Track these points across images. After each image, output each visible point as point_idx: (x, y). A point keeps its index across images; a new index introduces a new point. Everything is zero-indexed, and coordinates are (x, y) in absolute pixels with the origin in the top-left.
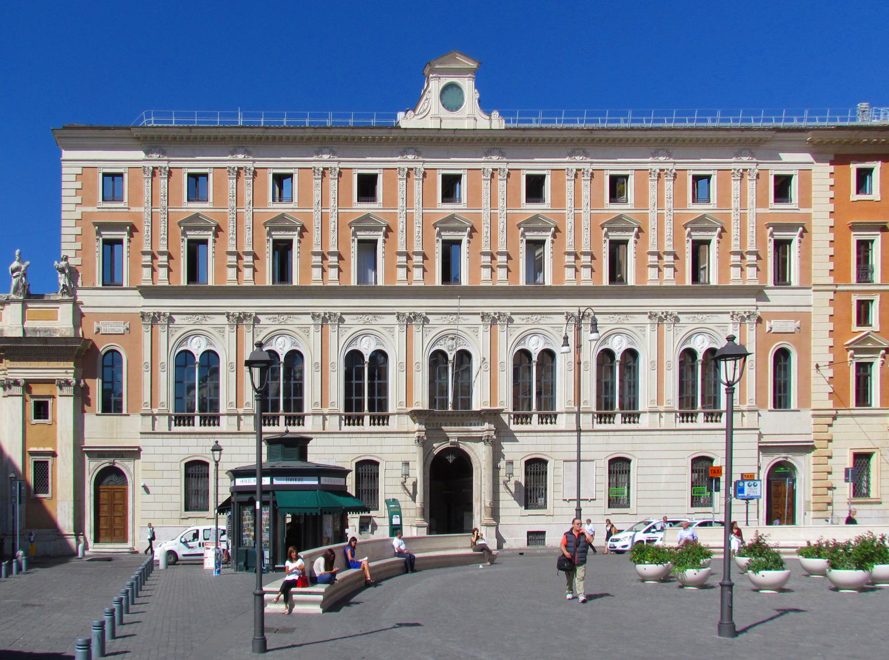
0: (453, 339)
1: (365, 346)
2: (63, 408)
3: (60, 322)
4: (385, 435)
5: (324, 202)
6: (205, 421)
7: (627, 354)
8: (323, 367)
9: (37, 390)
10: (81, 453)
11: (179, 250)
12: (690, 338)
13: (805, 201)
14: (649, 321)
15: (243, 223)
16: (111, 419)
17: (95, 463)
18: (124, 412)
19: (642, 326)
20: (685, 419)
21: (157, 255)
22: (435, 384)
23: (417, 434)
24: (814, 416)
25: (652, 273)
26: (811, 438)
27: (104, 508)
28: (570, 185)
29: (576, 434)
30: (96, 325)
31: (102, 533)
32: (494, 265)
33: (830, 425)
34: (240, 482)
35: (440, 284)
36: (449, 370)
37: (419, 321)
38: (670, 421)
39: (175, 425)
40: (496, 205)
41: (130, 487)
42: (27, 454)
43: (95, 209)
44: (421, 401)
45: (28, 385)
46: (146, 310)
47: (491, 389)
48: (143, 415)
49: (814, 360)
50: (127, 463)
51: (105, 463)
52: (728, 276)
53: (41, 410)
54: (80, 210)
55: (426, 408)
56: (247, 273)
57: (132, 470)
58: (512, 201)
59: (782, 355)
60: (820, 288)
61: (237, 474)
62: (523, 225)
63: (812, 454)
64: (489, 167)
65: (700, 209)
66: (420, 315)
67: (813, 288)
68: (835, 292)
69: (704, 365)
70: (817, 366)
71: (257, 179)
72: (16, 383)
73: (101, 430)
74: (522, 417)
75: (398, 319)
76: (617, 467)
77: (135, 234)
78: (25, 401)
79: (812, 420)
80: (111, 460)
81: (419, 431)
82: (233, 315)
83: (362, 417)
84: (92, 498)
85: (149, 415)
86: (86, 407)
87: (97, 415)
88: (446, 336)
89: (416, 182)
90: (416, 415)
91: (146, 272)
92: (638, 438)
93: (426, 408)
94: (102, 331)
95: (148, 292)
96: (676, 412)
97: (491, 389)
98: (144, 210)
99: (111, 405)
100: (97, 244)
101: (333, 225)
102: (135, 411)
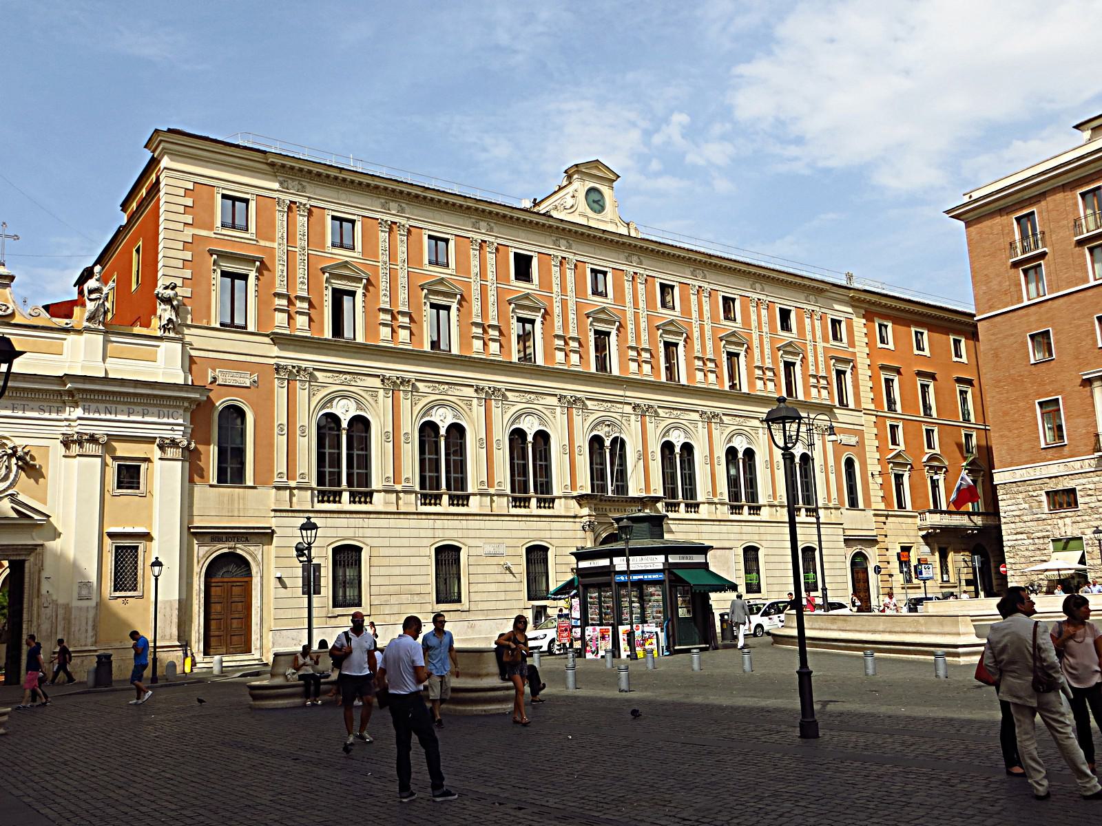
0: (609, 425)
1: (529, 425)
2: (164, 476)
3: (163, 365)
4: (554, 519)
5: (482, 273)
6: (454, 500)
7: (539, 438)
8: (395, 436)
9: (122, 450)
10: (193, 534)
11: (322, 298)
12: (668, 431)
13: (852, 343)
14: (475, 395)
15: (396, 280)
16: (228, 492)
17: (206, 548)
18: (249, 482)
19: (551, 408)
20: (518, 504)
21: (293, 299)
22: (450, 460)
23: (587, 519)
24: (875, 515)
25: (560, 356)
26: (874, 533)
27: (216, 608)
28: (694, 299)
29: (816, 526)
30: (210, 374)
31: (213, 642)
32: (395, 324)
33: (885, 523)
34: (584, 564)
35: (330, 337)
36: (606, 454)
37: (579, 405)
38: (410, 502)
39: (319, 502)
40: (486, 275)
41: (256, 581)
42: (105, 535)
43: (211, 234)
44: (584, 485)
45: (107, 445)
46: (283, 362)
47: (643, 479)
48: (278, 488)
49: (870, 469)
50: (252, 548)
51: (223, 548)
52: (810, 394)
53: (129, 476)
54: (190, 232)
55: (589, 492)
56: (403, 335)
57: (259, 557)
58: (501, 276)
59: (850, 463)
60: (867, 412)
61: (581, 555)
62: (662, 327)
63: (877, 547)
64: (632, 270)
65: (667, 315)
66: (579, 399)
67: (864, 411)
68: (876, 416)
69: (447, 438)
70: (872, 475)
71: (312, 219)
72: (93, 439)
73: (219, 506)
74: (672, 506)
75: (560, 401)
76: (534, 555)
77: (371, 288)
78: (104, 464)
79: (874, 519)
80: (232, 544)
81: (589, 515)
82: (389, 379)
83: (340, 493)
84: (202, 595)
85: (286, 488)
86: (196, 478)
87: (211, 486)
88: (603, 422)
89: (568, 271)
90: (581, 499)
91: (280, 318)
92: (764, 529)
93: (589, 492)
94: (220, 381)
95: (277, 339)
96: (312, 489)
97: (643, 479)
98: (278, 246)
99: (231, 472)
100: (213, 276)
101: (492, 299)
102: (265, 483)
